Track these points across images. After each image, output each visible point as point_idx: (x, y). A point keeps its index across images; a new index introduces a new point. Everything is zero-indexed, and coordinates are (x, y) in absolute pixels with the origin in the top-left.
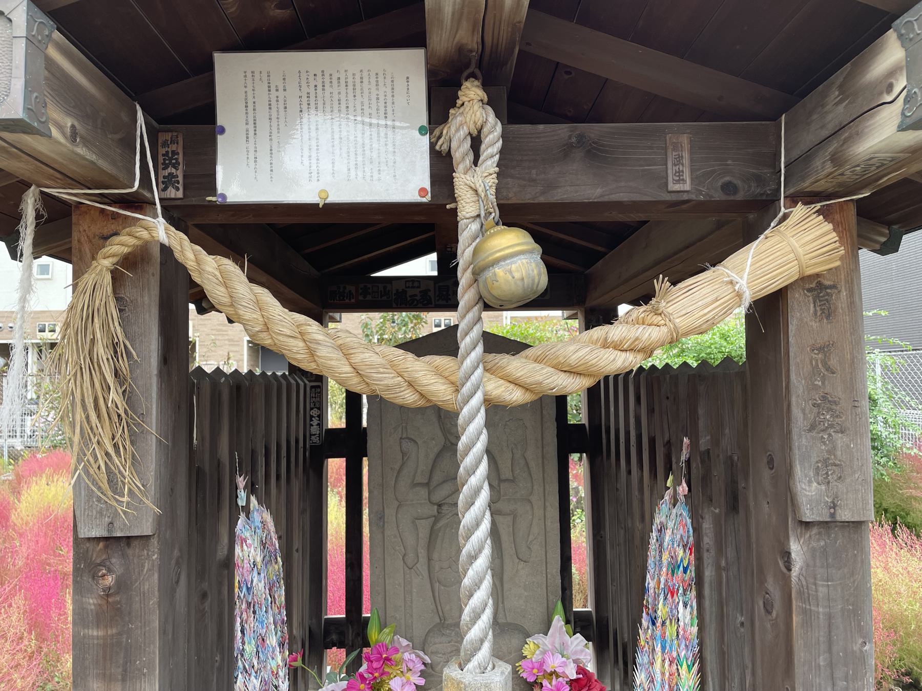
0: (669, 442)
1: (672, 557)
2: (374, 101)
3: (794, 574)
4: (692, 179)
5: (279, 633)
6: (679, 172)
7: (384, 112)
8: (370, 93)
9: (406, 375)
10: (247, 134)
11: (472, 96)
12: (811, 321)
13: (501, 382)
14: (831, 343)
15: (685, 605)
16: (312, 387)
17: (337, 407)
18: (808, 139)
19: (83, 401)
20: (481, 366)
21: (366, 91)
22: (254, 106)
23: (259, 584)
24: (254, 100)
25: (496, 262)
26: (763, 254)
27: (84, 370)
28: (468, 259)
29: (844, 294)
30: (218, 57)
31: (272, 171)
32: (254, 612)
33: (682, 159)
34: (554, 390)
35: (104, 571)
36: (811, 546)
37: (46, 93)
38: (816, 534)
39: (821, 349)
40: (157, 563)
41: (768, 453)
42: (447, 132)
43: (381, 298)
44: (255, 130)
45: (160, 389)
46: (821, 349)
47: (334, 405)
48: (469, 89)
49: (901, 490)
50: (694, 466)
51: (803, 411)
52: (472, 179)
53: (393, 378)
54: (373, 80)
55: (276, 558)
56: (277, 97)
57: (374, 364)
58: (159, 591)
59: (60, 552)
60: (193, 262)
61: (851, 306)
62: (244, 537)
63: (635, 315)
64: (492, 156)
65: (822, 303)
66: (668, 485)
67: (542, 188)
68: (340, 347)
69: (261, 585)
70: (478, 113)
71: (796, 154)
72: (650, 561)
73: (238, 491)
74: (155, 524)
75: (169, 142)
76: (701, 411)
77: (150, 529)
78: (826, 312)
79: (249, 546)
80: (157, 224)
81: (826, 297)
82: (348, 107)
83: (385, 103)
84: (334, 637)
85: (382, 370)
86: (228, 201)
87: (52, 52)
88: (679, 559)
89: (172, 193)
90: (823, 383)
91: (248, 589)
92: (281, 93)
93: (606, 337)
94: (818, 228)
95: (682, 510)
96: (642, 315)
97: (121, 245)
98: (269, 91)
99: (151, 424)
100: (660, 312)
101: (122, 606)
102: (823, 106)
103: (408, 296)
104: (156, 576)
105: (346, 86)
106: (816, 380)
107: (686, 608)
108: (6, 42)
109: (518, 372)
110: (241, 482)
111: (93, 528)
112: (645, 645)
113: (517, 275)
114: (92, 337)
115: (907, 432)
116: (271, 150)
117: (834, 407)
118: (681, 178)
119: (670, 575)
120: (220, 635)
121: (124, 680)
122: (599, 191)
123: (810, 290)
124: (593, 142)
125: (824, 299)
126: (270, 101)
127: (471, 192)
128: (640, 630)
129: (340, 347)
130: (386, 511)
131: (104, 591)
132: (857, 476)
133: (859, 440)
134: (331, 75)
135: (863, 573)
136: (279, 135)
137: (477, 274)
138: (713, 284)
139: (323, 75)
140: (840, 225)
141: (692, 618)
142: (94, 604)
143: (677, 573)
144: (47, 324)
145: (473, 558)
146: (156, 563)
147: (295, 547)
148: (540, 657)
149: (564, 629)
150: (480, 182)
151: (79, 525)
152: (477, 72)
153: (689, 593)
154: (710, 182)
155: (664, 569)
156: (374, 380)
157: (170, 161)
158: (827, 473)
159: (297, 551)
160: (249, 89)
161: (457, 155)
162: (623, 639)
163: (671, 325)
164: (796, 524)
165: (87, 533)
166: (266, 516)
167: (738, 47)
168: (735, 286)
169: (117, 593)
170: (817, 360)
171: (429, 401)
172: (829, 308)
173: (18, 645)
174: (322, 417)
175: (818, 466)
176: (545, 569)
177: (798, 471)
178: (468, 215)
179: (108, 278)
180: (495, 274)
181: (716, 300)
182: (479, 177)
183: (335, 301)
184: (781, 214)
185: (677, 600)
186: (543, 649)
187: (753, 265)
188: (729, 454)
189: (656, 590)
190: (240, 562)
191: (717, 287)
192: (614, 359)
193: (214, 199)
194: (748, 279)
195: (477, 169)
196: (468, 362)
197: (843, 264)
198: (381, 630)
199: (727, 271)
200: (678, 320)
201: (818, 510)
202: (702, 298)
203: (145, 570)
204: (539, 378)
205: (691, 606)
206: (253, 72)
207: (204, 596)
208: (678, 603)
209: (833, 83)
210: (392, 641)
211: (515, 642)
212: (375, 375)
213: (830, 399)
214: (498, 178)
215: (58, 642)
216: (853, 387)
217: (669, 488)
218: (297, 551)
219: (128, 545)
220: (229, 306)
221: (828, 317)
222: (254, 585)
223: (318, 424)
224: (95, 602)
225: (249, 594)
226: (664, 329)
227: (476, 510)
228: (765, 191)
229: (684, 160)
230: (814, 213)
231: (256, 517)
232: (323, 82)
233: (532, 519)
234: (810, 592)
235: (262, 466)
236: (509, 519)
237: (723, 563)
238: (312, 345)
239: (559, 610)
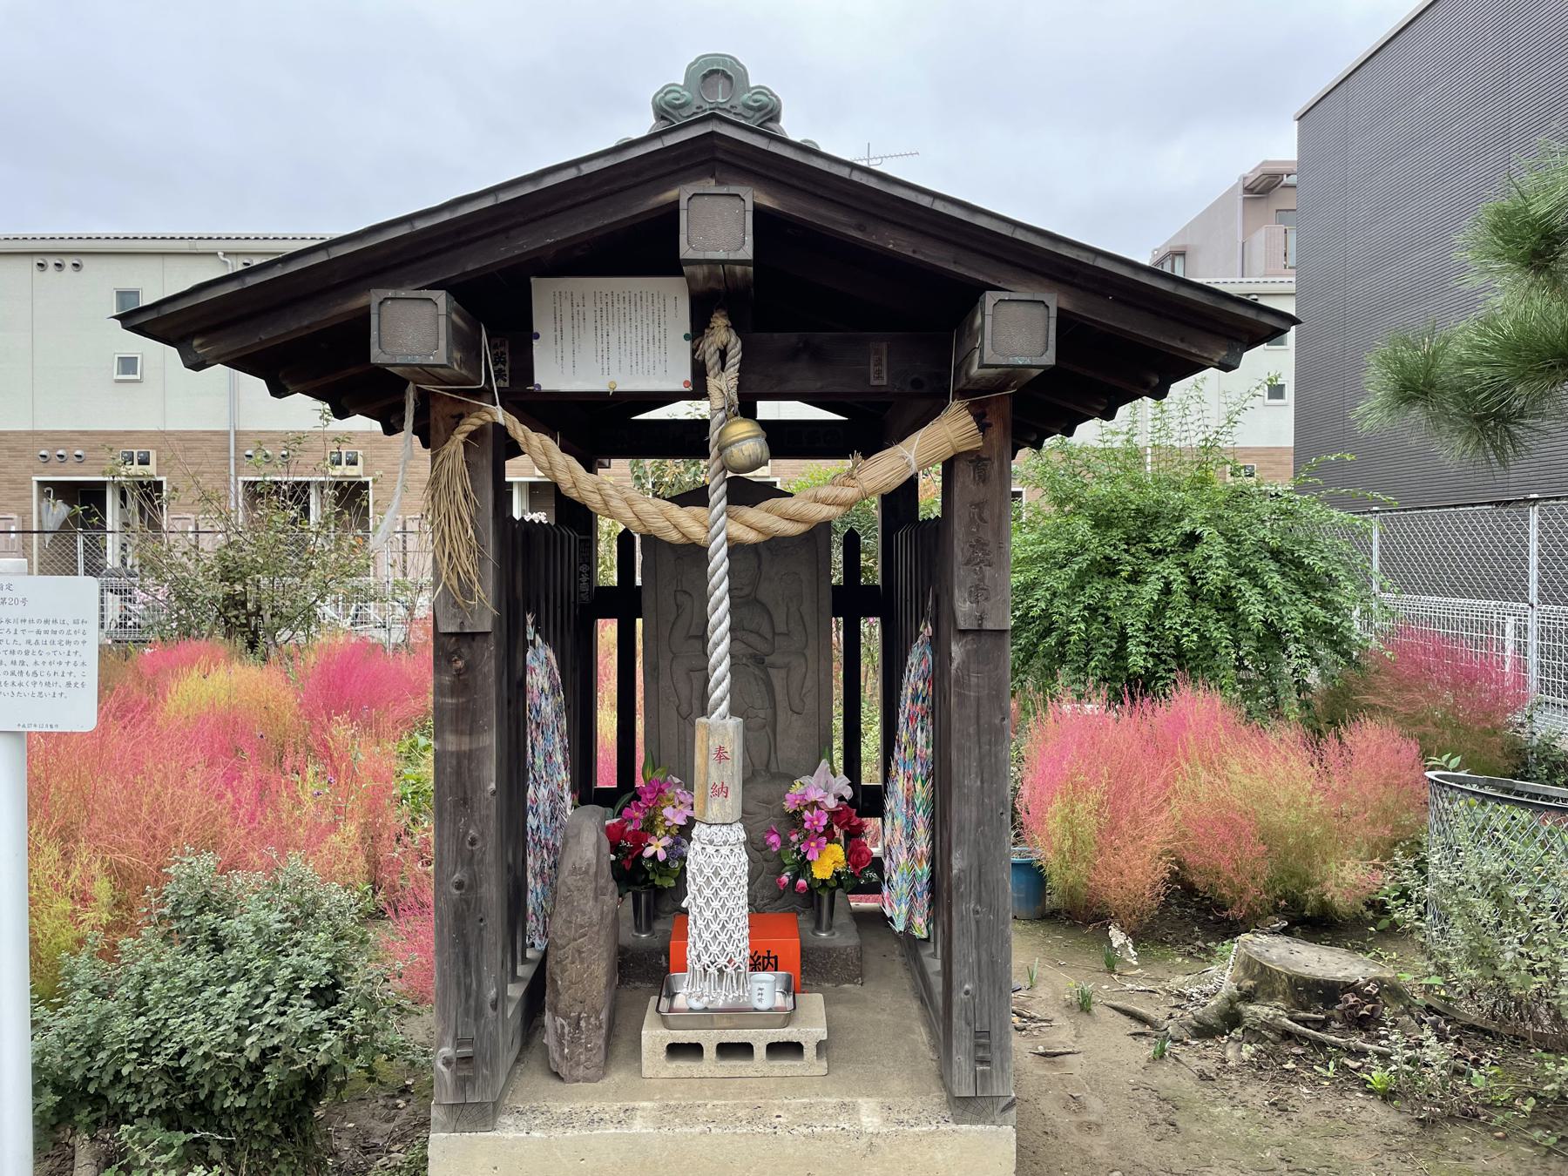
2: (650, 314)
15: (922, 729)
20: (725, 514)
21: (644, 307)
25: (733, 443)
29: (996, 464)
40: (494, 653)
68: (626, 500)
69: (549, 709)
89: (502, 384)
92: (581, 308)
97: (471, 424)
104: (493, 661)
110: (530, 619)
113: (746, 453)
121: (470, 734)
122: (819, 384)
123: (971, 462)
129: (626, 500)
144: (135, 452)
145: (717, 645)
160: (558, 305)
161: (709, 364)
169: (465, 673)
171: (689, 539)
172: (985, 474)
174: (591, 573)
181: (892, 469)
193: (531, 388)
196: (715, 511)
205: (928, 731)
219: (473, 640)
221: (984, 481)
223: (588, 581)
226: (856, 489)
231: (542, 653)
238: (607, 498)
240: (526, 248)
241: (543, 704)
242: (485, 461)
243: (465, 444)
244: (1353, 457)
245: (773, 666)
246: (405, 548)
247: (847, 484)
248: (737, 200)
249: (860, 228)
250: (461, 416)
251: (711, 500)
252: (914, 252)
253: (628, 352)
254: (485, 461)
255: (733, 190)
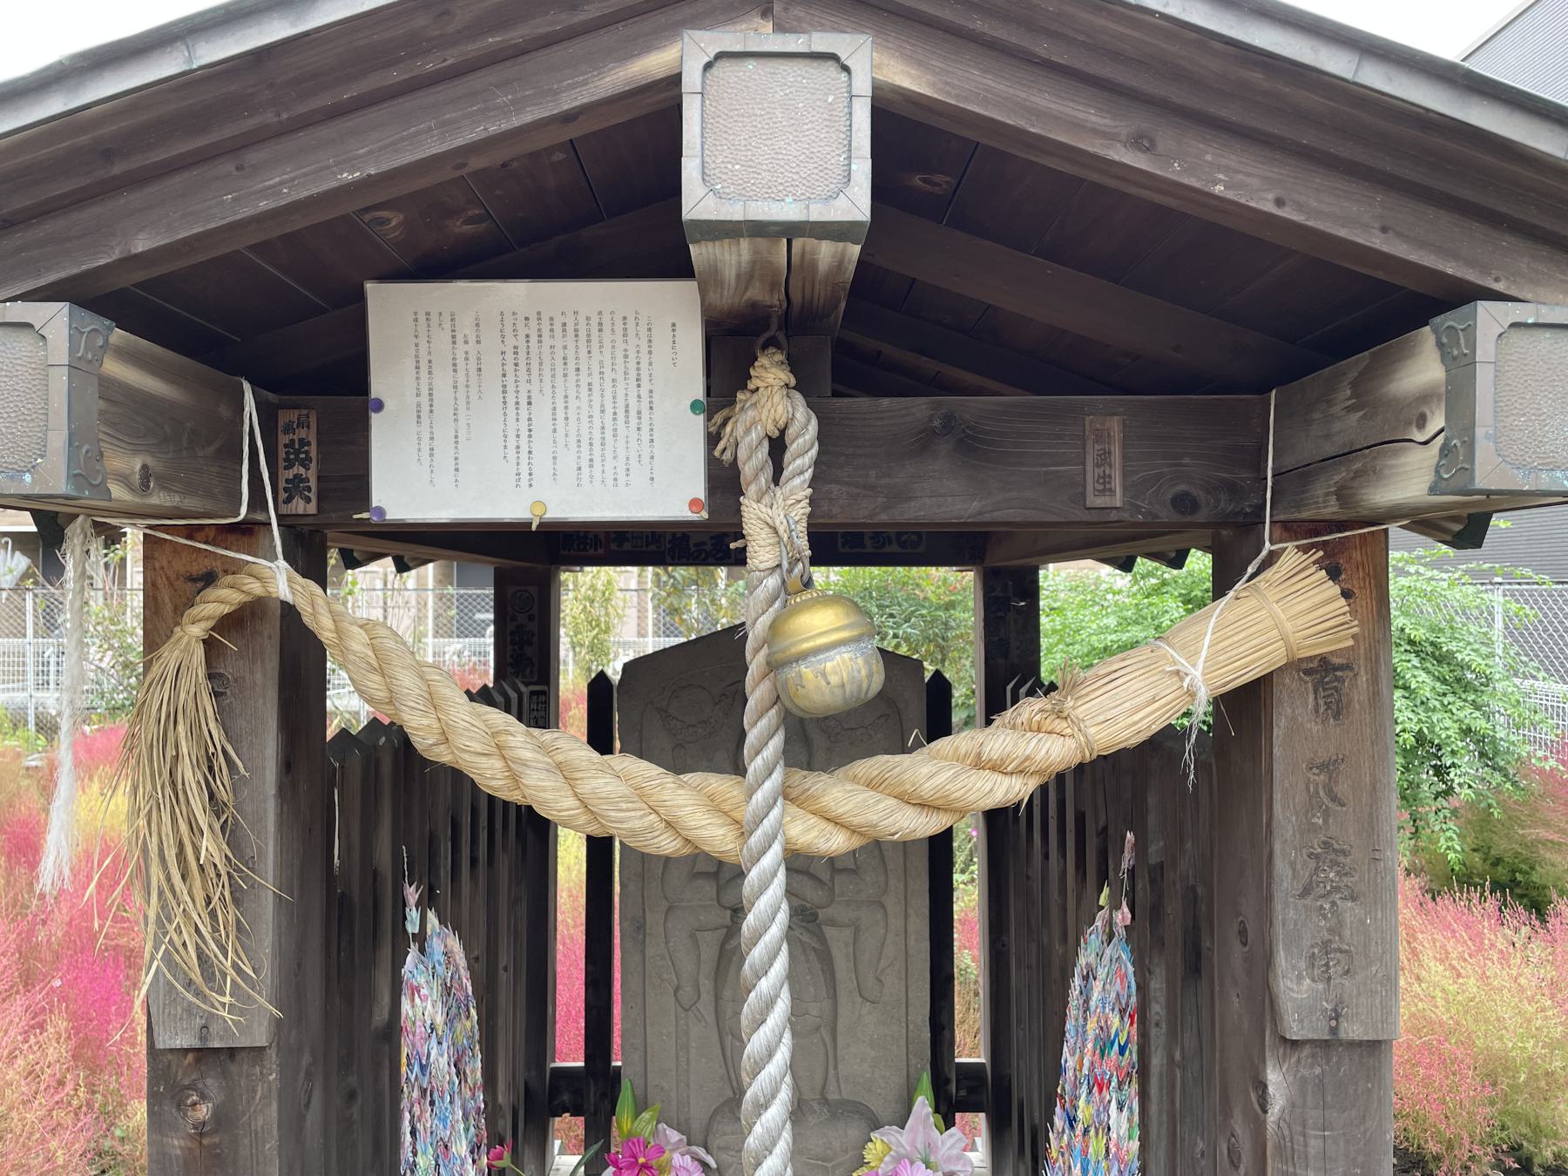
0: (1105, 829)
1: (1102, 1028)
2: (620, 360)
3: (1272, 1119)
4: (1125, 488)
5: (472, 1129)
6: (1104, 478)
7: (635, 377)
8: (613, 347)
9: (662, 811)
10: (418, 411)
11: (771, 381)
12: (1310, 721)
13: (812, 821)
14: (1341, 756)
15: (1120, 1108)
16: (532, 693)
17: (583, 652)
18: (1308, 448)
19: (161, 850)
22: (430, 367)
23: (440, 1059)
24: (430, 358)
25: (803, 656)
26: (1228, 629)
27: (162, 807)
28: (762, 634)
29: (1363, 678)
30: (370, 287)
31: (457, 470)
32: (432, 1103)
33: (1109, 457)
34: (896, 837)
35: (195, 1098)
36: (1299, 1075)
37: (102, 436)
38: (1307, 1057)
39: (1323, 767)
40: (276, 1086)
41: (1240, 918)
42: (732, 430)
43: (647, 546)
44: (431, 406)
45: (280, 815)
46: (1323, 767)
47: (578, 649)
48: (766, 368)
49: (1523, 829)
50: (1140, 886)
51: (1293, 864)
52: (769, 510)
53: (641, 817)
54: (619, 327)
55: (468, 1010)
56: (466, 353)
57: (612, 796)
58: (279, 1128)
59: (124, 914)
60: (331, 631)
61: (1374, 699)
62: (415, 984)
63: (1027, 716)
64: (802, 473)
65: (1329, 692)
66: (1101, 903)
67: (885, 500)
69: (444, 1061)
70: (780, 409)
71: (1290, 461)
72: (1070, 1025)
73: (407, 910)
74: (272, 1029)
75: (295, 426)
76: (1152, 800)
77: (264, 1038)
78: (1334, 707)
79: (423, 999)
80: (276, 570)
81: (1335, 684)
82: (578, 369)
83: (638, 363)
84: (566, 1097)
85: (624, 806)
86: (387, 518)
87: (114, 368)
88: (1113, 1032)
89: (299, 506)
90: (1326, 821)
91: (423, 1068)
93: (980, 753)
94: (1317, 590)
95: (1120, 952)
96: (1038, 718)
97: (219, 601)
98: (454, 343)
99: (266, 873)
100: (1065, 714)
101: (223, 1151)
102: (1329, 403)
103: (691, 546)
104: (275, 1106)
105: (577, 336)
106: (1314, 816)
107: (1121, 1111)
108: (37, 371)
109: (841, 807)
110: (412, 894)
111: (177, 1034)
112: (1058, 1157)
113: (834, 680)
114: (174, 753)
115: (1538, 736)
116: (456, 437)
117: (1341, 859)
118: (1107, 486)
119: (1097, 1057)
120: (377, 1146)
122: (976, 505)
124: (968, 427)
125: (1330, 686)
126: (454, 359)
127: (767, 530)
128: (1050, 1134)
130: (649, 916)
131: (195, 1127)
132: (1374, 969)
133: (1379, 912)
134: (552, 319)
135: (1380, 1119)
136: (469, 412)
137: (774, 667)
138: (1146, 675)
139: (539, 319)
140: (1360, 569)
141: (1131, 1127)
142: (180, 1147)
143: (1109, 1054)
145: (762, 1107)
146: (274, 1087)
147: (503, 962)
148: (892, 1167)
149: (932, 1119)
150: (782, 516)
151: (156, 1028)
152: (781, 337)
153: (1126, 1087)
154: (1154, 492)
155: (1090, 1046)
156: (612, 822)
157: (297, 455)
158: (1327, 965)
159: (506, 969)
160: (423, 346)
161: (747, 470)
162: (1032, 1118)
163: (1082, 739)
164: (1277, 1041)
165: (168, 1042)
166: (453, 943)
167: (1202, 282)
168: (1182, 680)
169: (214, 1131)
170: (1317, 784)
173: (56, 1092)
175: (1314, 954)
176: (904, 1015)
177: (1282, 959)
178: (762, 566)
179: (199, 652)
180: (800, 675)
181: (1154, 700)
182: (780, 509)
183: (572, 552)
184: (1264, 553)
185: (1108, 1097)
186: (896, 1152)
187: (1213, 645)
188: (1191, 882)
189: (1077, 1073)
190: (409, 1024)
191: (1155, 678)
192: (991, 790)
193: (365, 515)
194: (1204, 668)
195: (778, 491)
196: (759, 796)
197: (1363, 630)
198: (637, 1114)
199: (1170, 651)
200: (1092, 730)
201: (1311, 1022)
202: (1131, 696)
203: (258, 1097)
204: (872, 817)
205: (1130, 1108)
206: (428, 314)
207: (352, 1096)
208: (1110, 1102)
209: (1344, 374)
210: (655, 1133)
211: (853, 1132)
212: (612, 814)
213: (1336, 846)
214: (810, 504)
215: (122, 1074)
216: (1373, 829)
217: (1103, 908)
218: (506, 969)
220: (387, 703)
221: (1336, 716)
222: (431, 1060)
224: (182, 1143)
225: (424, 1075)
226: (1071, 743)
227: (768, 1033)
228: (1242, 509)
229: (1113, 458)
230: (1314, 563)
231: (436, 946)
232: (539, 330)
233: (886, 934)
234: (1296, 1146)
235: (446, 858)
236: (847, 933)
237: (1178, 1056)
239: (924, 1088)
240: (289, 195)
241: (434, 1053)
242: (259, 676)
243: (209, 644)
244: (1509, 524)
245: (832, 922)
246: (385, 611)
247: (1047, 725)
248: (831, 69)
249: (1139, 142)
250: (209, 579)
251: (751, 770)
252: (1279, 202)
253: (572, 440)
254: (259, 676)
255: (821, 42)
